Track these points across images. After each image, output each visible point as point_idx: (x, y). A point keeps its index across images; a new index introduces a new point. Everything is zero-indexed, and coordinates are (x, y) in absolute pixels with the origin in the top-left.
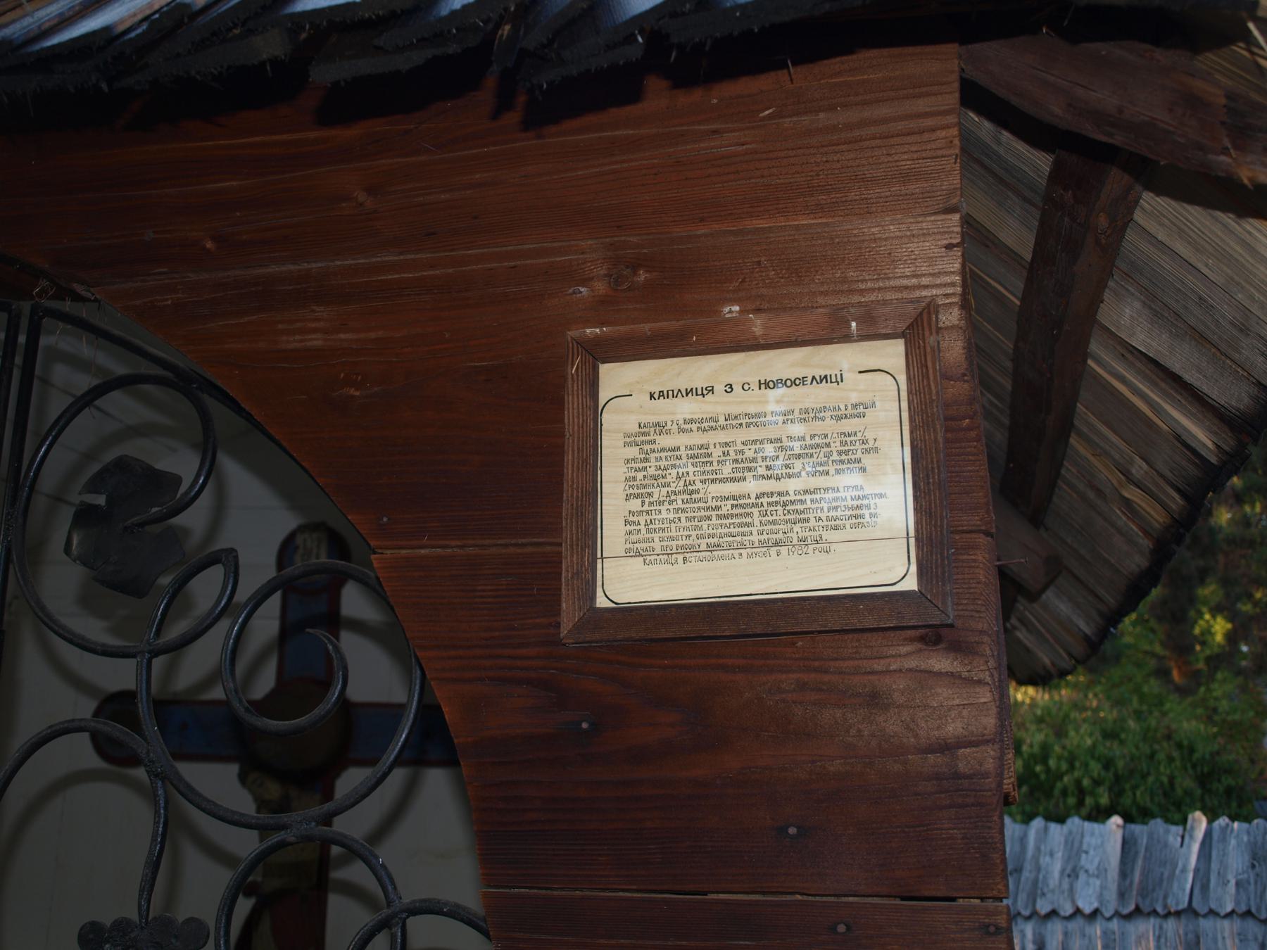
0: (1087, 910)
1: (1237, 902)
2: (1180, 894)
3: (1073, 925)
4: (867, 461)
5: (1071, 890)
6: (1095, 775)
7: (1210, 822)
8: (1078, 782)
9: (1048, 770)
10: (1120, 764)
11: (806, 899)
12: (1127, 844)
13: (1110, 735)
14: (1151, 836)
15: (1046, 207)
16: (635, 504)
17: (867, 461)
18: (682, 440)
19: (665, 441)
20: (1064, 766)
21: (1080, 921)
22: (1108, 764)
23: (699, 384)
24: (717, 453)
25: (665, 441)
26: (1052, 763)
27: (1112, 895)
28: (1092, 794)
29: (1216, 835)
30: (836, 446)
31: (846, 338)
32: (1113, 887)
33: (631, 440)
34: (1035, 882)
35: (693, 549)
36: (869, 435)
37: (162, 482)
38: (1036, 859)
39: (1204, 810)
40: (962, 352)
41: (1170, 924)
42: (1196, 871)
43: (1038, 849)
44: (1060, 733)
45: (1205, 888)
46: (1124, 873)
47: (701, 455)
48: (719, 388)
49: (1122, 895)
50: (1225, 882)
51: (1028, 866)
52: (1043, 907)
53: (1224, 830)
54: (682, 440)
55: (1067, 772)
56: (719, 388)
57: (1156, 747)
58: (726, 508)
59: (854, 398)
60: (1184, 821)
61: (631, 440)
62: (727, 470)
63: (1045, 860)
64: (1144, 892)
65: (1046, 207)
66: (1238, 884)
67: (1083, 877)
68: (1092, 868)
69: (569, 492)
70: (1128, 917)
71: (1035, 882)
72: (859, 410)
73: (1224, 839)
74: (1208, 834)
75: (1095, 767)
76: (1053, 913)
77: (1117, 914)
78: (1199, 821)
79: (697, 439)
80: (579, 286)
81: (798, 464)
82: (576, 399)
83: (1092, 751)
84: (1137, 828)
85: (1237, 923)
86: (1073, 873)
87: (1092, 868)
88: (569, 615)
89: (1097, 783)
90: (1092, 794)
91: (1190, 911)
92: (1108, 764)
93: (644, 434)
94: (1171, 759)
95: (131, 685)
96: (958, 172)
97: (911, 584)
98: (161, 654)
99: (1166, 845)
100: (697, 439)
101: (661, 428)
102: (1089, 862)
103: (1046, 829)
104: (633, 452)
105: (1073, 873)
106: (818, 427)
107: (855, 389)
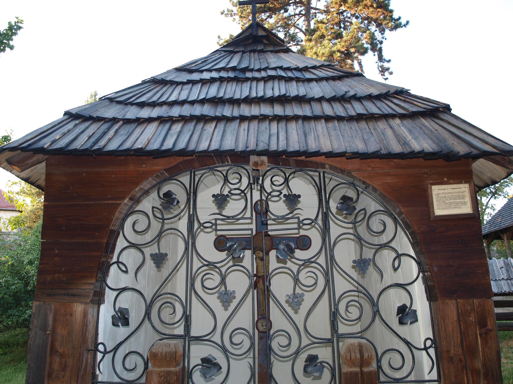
4: (465, 198)
11: (171, 297)
16: (438, 203)
17: (465, 198)
18: (443, 195)
19: (440, 195)
23: (444, 188)
24: (447, 197)
25: (440, 195)
30: (461, 196)
31: (463, 183)
33: (436, 195)
35: (445, 208)
36: (465, 195)
37: (351, 199)
40: (382, 122)
47: (445, 197)
48: (446, 189)
50: (260, 285)
54: (443, 195)
56: (446, 189)
58: (449, 203)
59: (463, 190)
61: (436, 195)
62: (448, 199)
69: (430, 204)
72: (464, 192)
79: (445, 195)
81: (457, 198)
82: (509, 218)
88: (432, 216)
93: (437, 195)
95: (268, 229)
97: (472, 212)
98: (128, 217)
100: (445, 195)
101: (440, 194)
104: (437, 197)
106: (459, 194)
107: (463, 189)
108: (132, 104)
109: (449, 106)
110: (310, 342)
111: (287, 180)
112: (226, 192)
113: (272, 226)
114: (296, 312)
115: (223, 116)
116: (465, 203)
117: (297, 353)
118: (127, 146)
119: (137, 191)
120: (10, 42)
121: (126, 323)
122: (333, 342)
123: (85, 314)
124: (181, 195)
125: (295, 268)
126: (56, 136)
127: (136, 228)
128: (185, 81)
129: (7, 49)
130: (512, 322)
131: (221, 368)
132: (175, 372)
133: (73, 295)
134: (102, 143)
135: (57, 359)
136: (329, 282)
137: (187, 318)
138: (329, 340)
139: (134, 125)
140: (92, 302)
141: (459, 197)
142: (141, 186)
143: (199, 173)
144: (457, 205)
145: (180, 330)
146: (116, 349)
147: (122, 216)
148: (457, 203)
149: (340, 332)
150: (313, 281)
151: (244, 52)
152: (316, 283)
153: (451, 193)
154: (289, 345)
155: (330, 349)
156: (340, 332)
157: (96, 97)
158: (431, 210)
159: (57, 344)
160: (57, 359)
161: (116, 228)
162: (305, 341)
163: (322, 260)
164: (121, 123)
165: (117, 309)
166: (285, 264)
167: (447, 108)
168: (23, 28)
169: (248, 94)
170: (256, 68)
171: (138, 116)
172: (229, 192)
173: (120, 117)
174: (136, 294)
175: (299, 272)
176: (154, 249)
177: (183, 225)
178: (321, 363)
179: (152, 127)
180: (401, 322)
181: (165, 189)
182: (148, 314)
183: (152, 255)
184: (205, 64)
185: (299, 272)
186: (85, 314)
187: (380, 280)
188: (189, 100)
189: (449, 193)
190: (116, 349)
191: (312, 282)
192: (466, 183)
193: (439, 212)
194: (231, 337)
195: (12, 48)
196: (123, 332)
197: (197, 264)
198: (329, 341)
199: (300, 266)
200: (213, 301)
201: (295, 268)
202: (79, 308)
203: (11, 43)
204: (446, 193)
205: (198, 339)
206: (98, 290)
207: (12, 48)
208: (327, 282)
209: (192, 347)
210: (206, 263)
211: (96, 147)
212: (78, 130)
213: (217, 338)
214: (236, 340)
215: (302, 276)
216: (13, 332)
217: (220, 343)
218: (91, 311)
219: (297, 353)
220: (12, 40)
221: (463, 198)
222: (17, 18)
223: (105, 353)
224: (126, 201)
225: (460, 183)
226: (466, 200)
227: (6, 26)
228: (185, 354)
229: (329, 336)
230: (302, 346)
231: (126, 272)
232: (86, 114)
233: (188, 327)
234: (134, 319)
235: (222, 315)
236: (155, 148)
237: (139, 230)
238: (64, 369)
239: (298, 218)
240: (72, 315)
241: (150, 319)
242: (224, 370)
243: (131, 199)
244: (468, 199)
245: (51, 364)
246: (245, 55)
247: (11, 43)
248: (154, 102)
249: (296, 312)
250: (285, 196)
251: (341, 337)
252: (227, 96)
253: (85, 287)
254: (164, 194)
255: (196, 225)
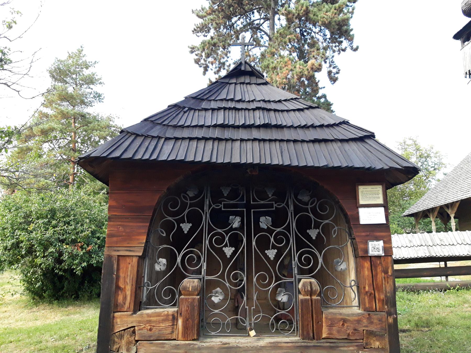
97: (383, 203)
109: (373, 133)
113: (428, 255)
116: (379, 198)
118: (128, 155)
132: (327, 327)
151: (236, 84)
153: (371, 191)
167: (371, 136)
168: (457, 37)
169: (244, 122)
170: (247, 100)
184: (210, 95)
188: (192, 125)
189: (369, 191)
216: (75, 251)
221: (378, 195)
226: (379, 196)
236: (164, 159)
244: (381, 196)
246: (236, 86)
252: (230, 123)
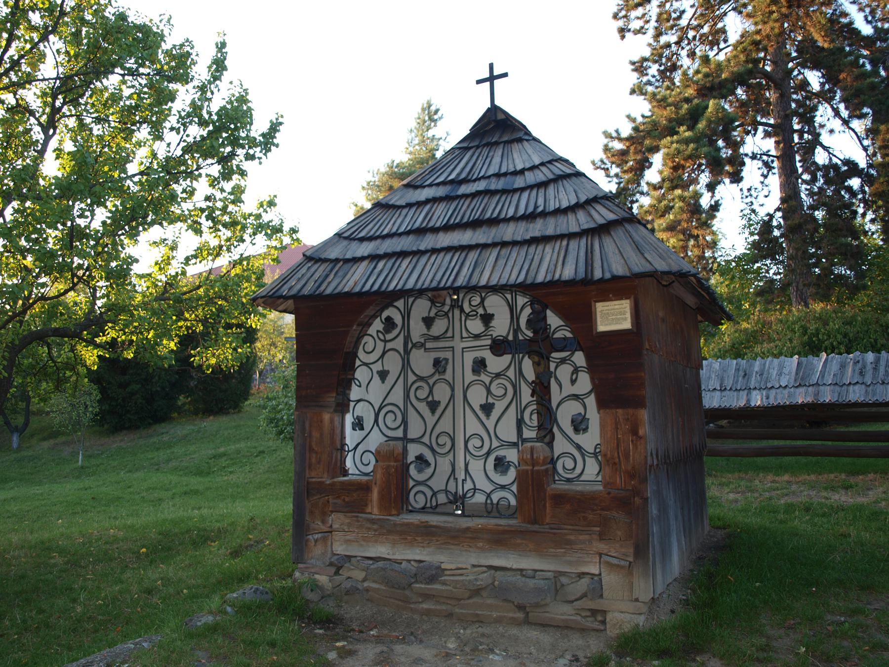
0: (783, 386)
1: (833, 380)
2: (814, 380)
3: (778, 391)
5: (779, 379)
6: (839, 340)
7: (827, 355)
8: (832, 344)
9: (819, 340)
10: (851, 335)
12: (799, 364)
13: (849, 323)
14: (807, 361)
15: (455, 297)
20: (825, 337)
21: (781, 389)
22: (845, 335)
26: (820, 336)
27: (792, 381)
28: (838, 348)
29: (829, 360)
32: (793, 378)
34: (767, 378)
38: (768, 370)
39: (826, 352)
41: (810, 389)
42: (821, 371)
43: (769, 367)
44: (826, 323)
45: (823, 377)
46: (797, 374)
47: (608, 313)
49: (795, 380)
51: (765, 373)
52: (769, 385)
53: (832, 358)
55: (827, 339)
57: (870, 327)
60: (818, 356)
63: (771, 371)
64: (802, 379)
65: (455, 297)
66: (834, 375)
67: (783, 375)
68: (786, 372)
70: (797, 387)
71: (767, 378)
72: (625, 308)
73: (832, 361)
74: (826, 360)
75: (839, 337)
76: (773, 387)
77: (793, 386)
78: (824, 355)
80: (829, 50)
83: (838, 330)
84: (803, 359)
85: (832, 387)
86: (780, 374)
87: (786, 372)
88: (632, 299)
89: (840, 343)
90: (838, 348)
91: (817, 384)
92: (845, 335)
94: (876, 331)
96: (593, 212)
99: (812, 364)
102: (786, 371)
103: (772, 361)
105: (780, 374)
108: (354, 239)
110: (500, 445)
111: (483, 300)
112: (432, 314)
114: (488, 419)
115: (418, 250)
116: (625, 319)
117: (488, 453)
119: (362, 318)
120: (274, 140)
121: (362, 428)
122: (518, 446)
123: (332, 421)
124: (398, 319)
125: (487, 380)
126: (293, 282)
127: (366, 350)
128: (404, 204)
129: (273, 148)
130: (887, 444)
131: (430, 464)
133: (321, 406)
134: (322, 288)
135: (314, 455)
136: (516, 392)
137: (405, 422)
138: (515, 443)
139: (350, 264)
140: (336, 411)
141: (621, 313)
142: (365, 314)
143: (411, 300)
144: (618, 321)
145: (399, 433)
146: (355, 448)
147: (355, 339)
148: (618, 319)
149: (524, 436)
150: (503, 392)
152: (505, 394)
154: (482, 446)
155: (516, 450)
156: (524, 436)
157: (431, 108)
158: (594, 327)
159: (313, 444)
160: (314, 455)
161: (351, 349)
162: (495, 443)
163: (511, 373)
164: (341, 263)
165: (355, 417)
166: (479, 376)
171: (354, 256)
172: (436, 314)
173: (341, 257)
174: (367, 403)
175: (491, 383)
176: (377, 367)
177: (399, 344)
178: (508, 462)
179: (362, 268)
180: (577, 430)
181: (385, 315)
182: (376, 421)
183: (378, 372)
185: (491, 383)
186: (332, 421)
187: (559, 390)
189: (612, 309)
190: (355, 448)
191: (502, 392)
192: (626, 299)
193: (602, 327)
194: (437, 438)
195: (277, 146)
196: (360, 435)
197: (411, 378)
198: (514, 445)
199: (493, 378)
200: (423, 408)
201: (487, 380)
202: (326, 417)
203: (275, 141)
204: (609, 310)
205: (413, 441)
206: (341, 401)
207: (277, 146)
208: (408, 392)
209: (408, 445)
210: (494, 375)
211: (317, 292)
212: (313, 270)
213: (426, 440)
214: (441, 441)
215: (493, 388)
217: (428, 443)
218: (337, 419)
219: (488, 453)
220: (275, 138)
222: (268, 141)
223: (349, 451)
224: (354, 327)
225: (622, 299)
227: (268, 125)
228: (405, 451)
229: (515, 440)
230: (492, 448)
231: (360, 386)
232: (316, 256)
233: (405, 431)
234: (368, 422)
235: (431, 420)
237: (371, 350)
238: (319, 463)
239: (492, 335)
240: (321, 422)
241: (378, 425)
242: (433, 465)
243: (358, 325)
245: (310, 459)
247: (275, 141)
248: (371, 236)
249: (488, 419)
250: (481, 315)
251: (524, 441)
253: (329, 399)
254: (385, 319)
255: (410, 345)
